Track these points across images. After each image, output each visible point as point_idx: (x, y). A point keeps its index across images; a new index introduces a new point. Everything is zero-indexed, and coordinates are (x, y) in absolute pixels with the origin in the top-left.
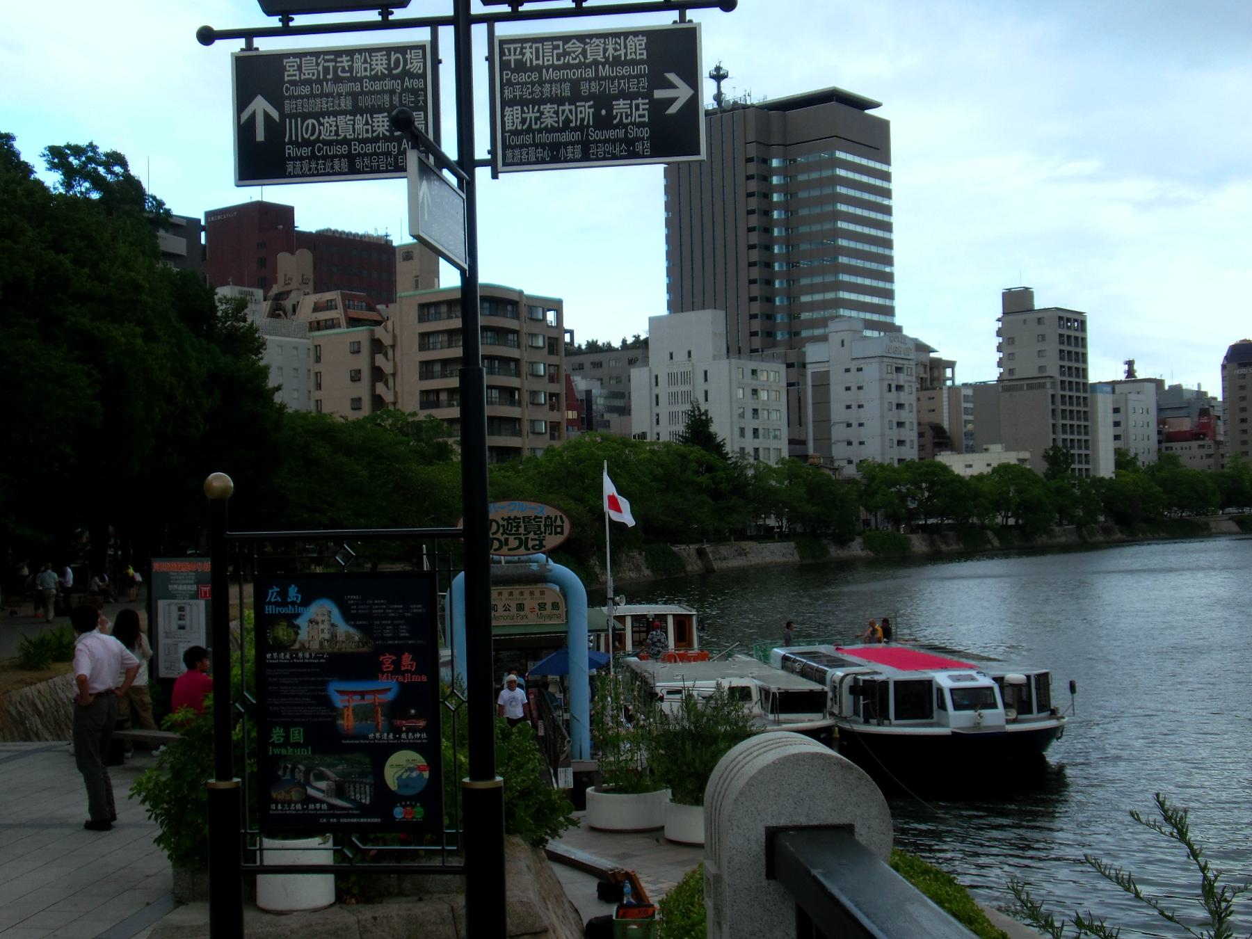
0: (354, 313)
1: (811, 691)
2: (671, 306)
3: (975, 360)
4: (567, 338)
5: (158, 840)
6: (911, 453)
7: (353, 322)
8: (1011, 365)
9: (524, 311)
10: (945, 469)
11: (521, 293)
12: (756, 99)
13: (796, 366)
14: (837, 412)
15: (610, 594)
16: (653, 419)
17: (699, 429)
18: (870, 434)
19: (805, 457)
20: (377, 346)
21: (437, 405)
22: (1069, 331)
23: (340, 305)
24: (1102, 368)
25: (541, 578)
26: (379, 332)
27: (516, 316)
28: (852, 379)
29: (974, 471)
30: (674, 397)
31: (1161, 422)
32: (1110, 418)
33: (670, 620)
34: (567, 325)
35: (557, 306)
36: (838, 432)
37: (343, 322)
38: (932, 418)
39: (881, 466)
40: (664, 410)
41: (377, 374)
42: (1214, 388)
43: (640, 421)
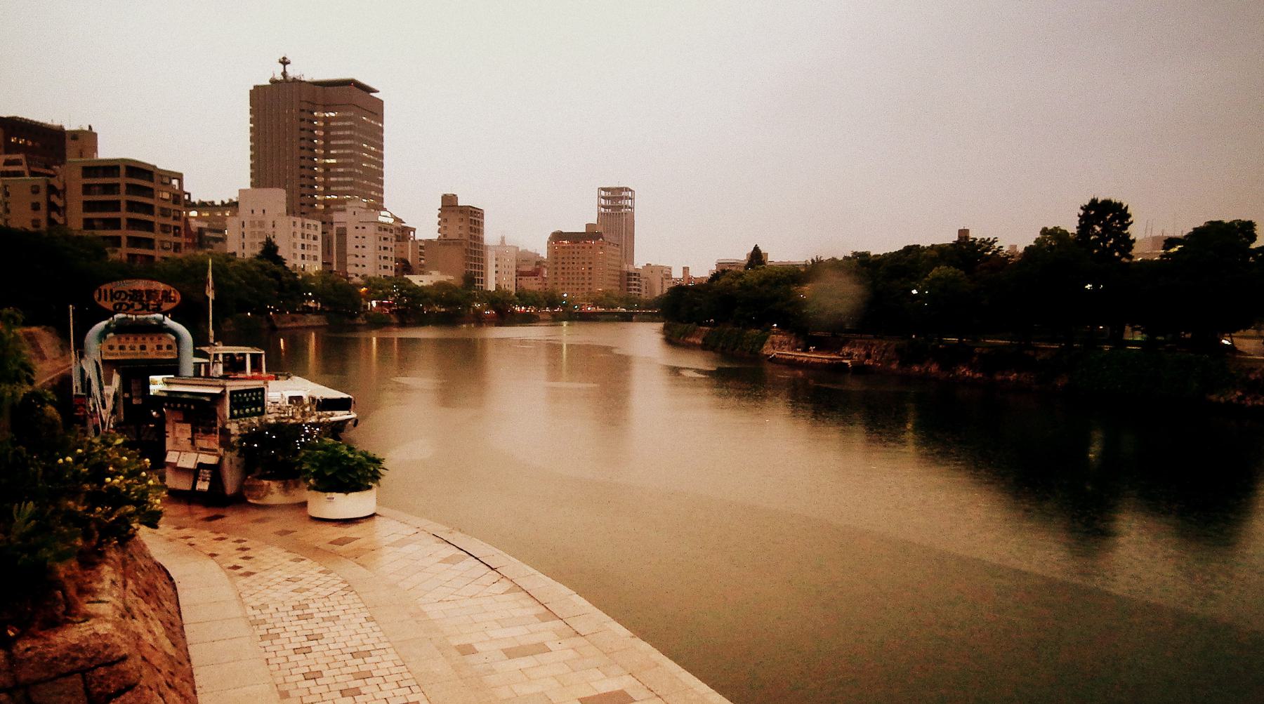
0: (33, 169)
1: (342, 399)
2: (252, 185)
3: (427, 227)
4: (186, 197)
5: (1106, 216)
6: (391, 273)
7: (33, 174)
8: (445, 232)
9: (156, 178)
10: (410, 281)
11: (154, 167)
12: (307, 78)
13: (327, 223)
14: (350, 249)
15: (212, 341)
16: (241, 244)
17: (270, 250)
18: (366, 262)
19: (331, 272)
20: (51, 189)
21: (93, 228)
22: (473, 217)
23: (24, 163)
24: (491, 234)
25: (161, 329)
26: (53, 181)
27: (151, 180)
28: (360, 232)
29: (424, 284)
30: (253, 235)
31: (517, 266)
32: (494, 263)
33: (248, 357)
34: (186, 189)
35: (180, 177)
36: (351, 260)
37: (27, 173)
38: (401, 256)
39: (374, 278)
40: (247, 241)
41: (52, 207)
42: (544, 254)
43: (232, 246)
